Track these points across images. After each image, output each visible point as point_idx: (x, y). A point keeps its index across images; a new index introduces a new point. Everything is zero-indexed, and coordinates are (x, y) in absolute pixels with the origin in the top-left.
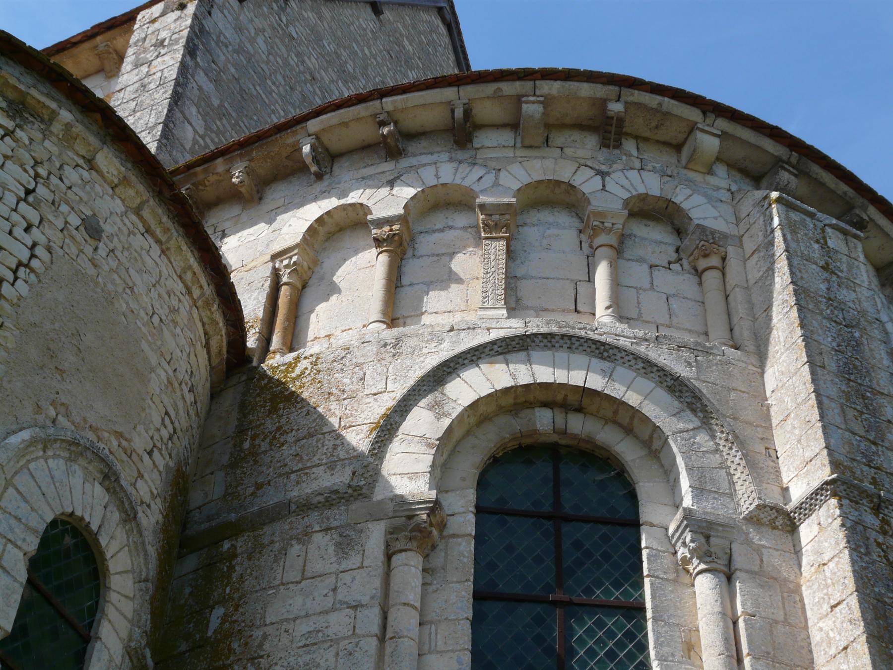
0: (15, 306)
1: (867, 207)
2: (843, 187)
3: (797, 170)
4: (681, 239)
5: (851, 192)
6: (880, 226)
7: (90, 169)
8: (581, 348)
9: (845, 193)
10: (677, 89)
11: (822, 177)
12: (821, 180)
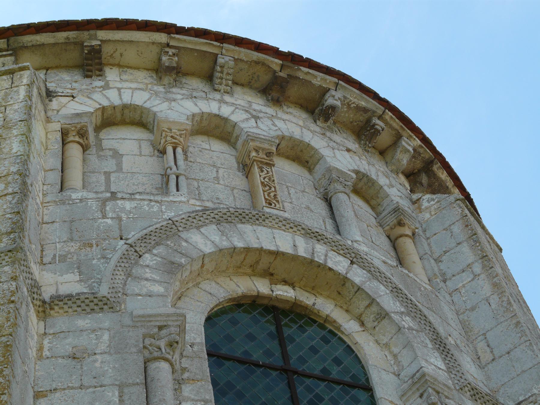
0: (118, 292)
1: (96, 34)
2: (62, 36)
3: (11, 50)
4: (384, 158)
5: (72, 34)
6: (118, 41)
7: (254, 301)
8: (291, 230)
9: (68, 38)
10: (260, 43)
11: (37, 41)
12: (38, 43)
